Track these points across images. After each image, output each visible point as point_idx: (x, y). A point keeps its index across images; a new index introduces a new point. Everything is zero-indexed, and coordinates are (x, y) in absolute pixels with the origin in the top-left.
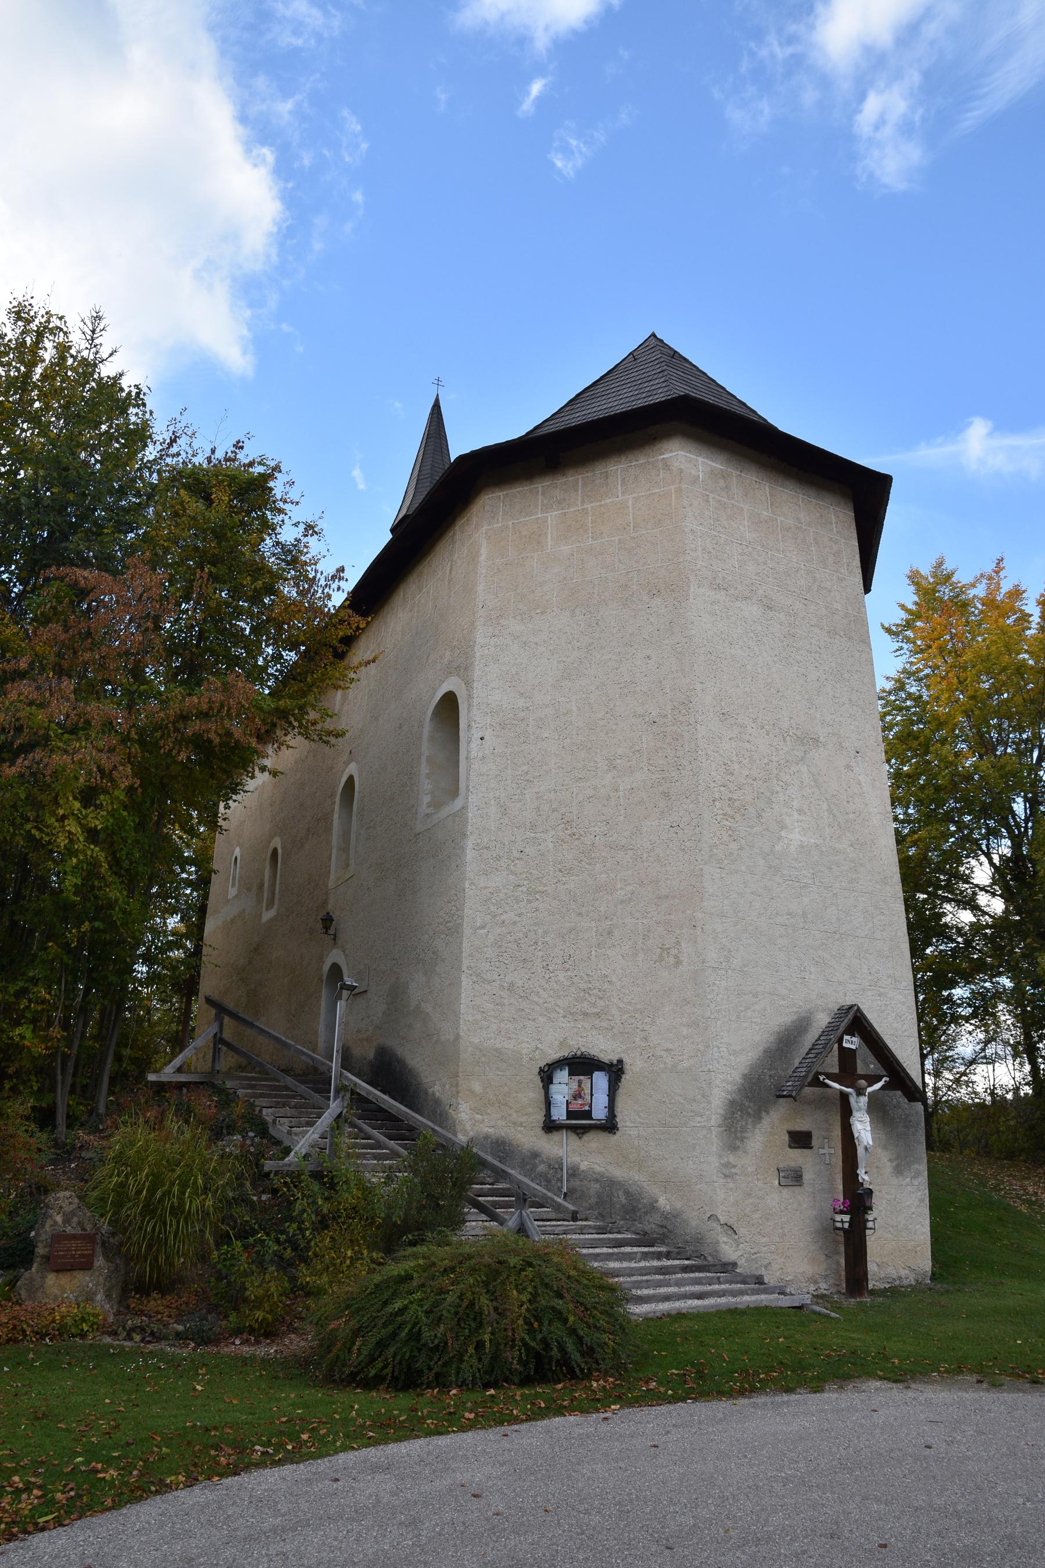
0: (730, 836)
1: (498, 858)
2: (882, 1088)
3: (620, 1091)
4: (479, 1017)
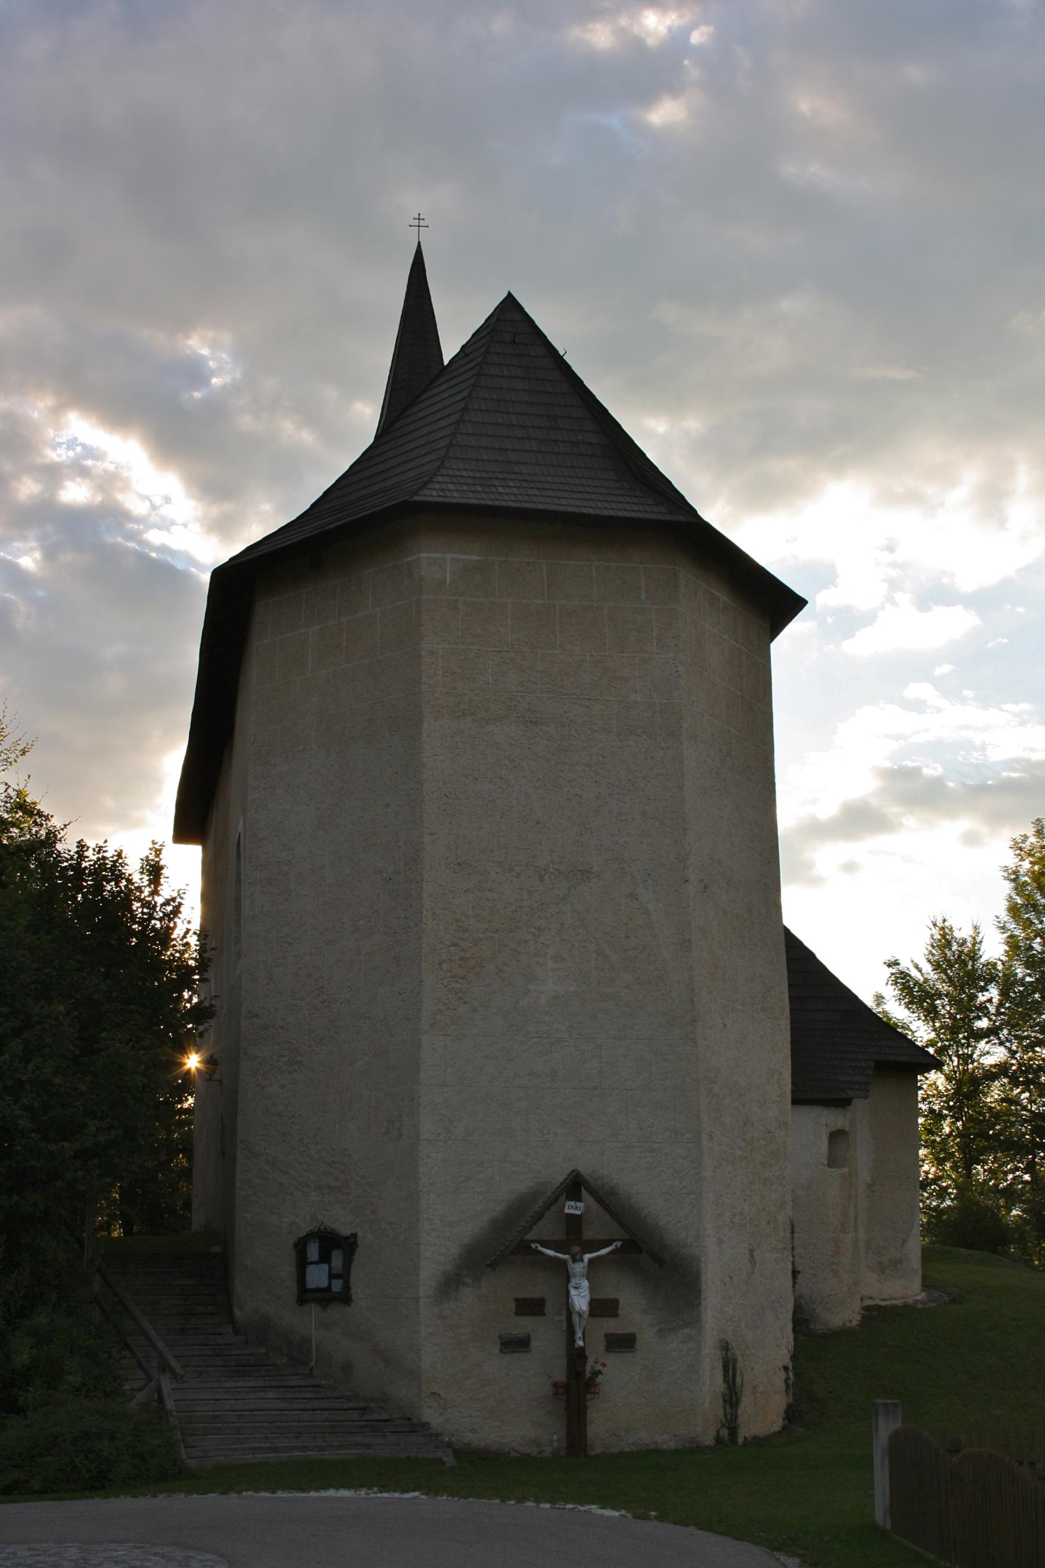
0: (460, 999)
2: (609, 1253)
3: (354, 1265)
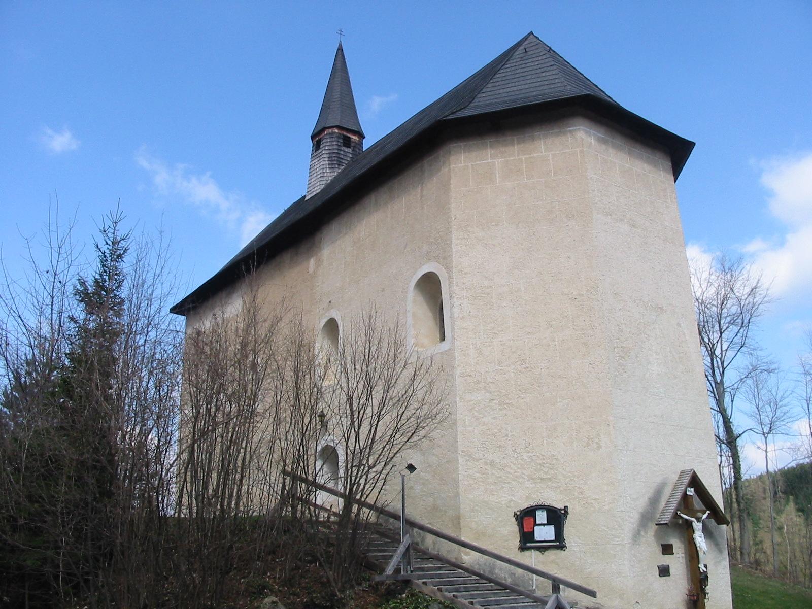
0: (623, 369)
1: (478, 382)
4: (471, 482)
